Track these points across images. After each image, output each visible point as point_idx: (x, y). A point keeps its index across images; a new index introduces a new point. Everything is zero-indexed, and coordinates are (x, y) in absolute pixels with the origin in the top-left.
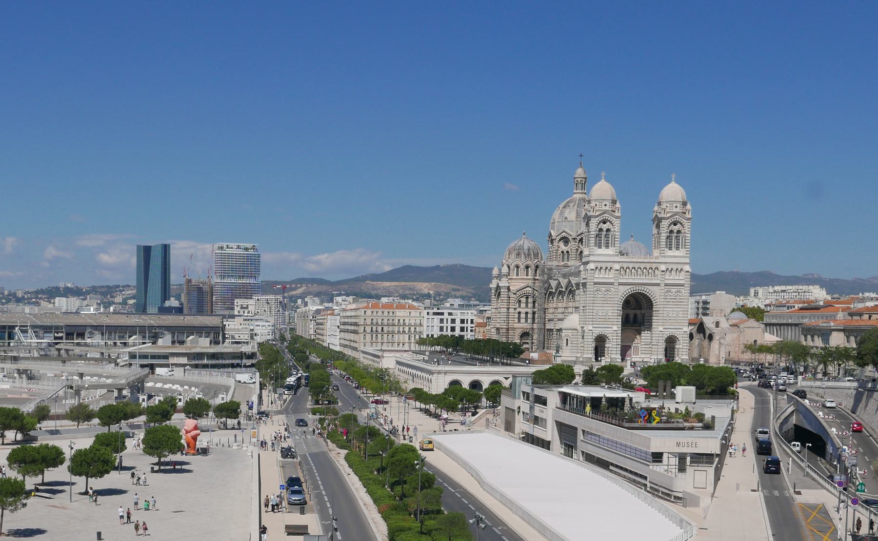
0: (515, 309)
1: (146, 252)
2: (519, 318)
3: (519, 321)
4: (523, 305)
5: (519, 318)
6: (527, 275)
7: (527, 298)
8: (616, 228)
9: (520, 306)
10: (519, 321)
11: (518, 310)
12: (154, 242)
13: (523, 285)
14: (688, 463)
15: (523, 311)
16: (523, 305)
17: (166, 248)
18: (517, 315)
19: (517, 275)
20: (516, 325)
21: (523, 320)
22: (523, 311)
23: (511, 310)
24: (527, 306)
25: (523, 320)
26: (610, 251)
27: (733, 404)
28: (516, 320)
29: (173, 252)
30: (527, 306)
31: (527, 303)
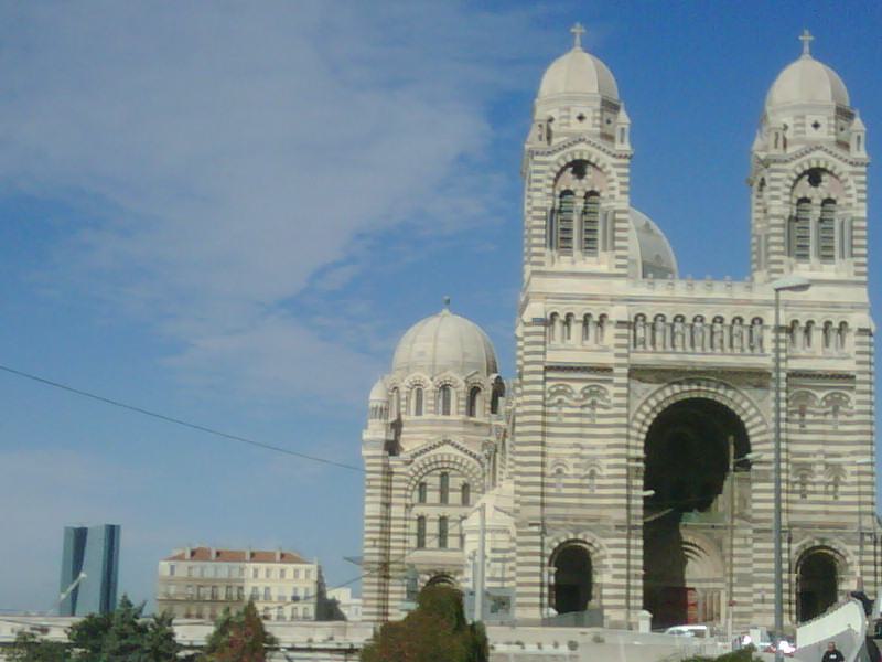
0: (408, 507)
1: (80, 537)
2: (421, 534)
3: (421, 545)
4: (432, 496)
5: (421, 534)
6: (446, 412)
7: (444, 476)
8: (614, 191)
9: (422, 500)
10: (421, 545)
11: (419, 510)
12: (95, 522)
13: (435, 439)
14: (731, 467)
15: (432, 512)
16: (432, 496)
17: (112, 532)
18: (413, 527)
19: (419, 412)
20: (416, 556)
21: (432, 542)
22: (432, 512)
23: (397, 511)
24: (444, 500)
25: (432, 542)
26: (602, 262)
27: (313, 618)
28: (413, 541)
29: (125, 541)
30: (444, 500)
31: (444, 491)
